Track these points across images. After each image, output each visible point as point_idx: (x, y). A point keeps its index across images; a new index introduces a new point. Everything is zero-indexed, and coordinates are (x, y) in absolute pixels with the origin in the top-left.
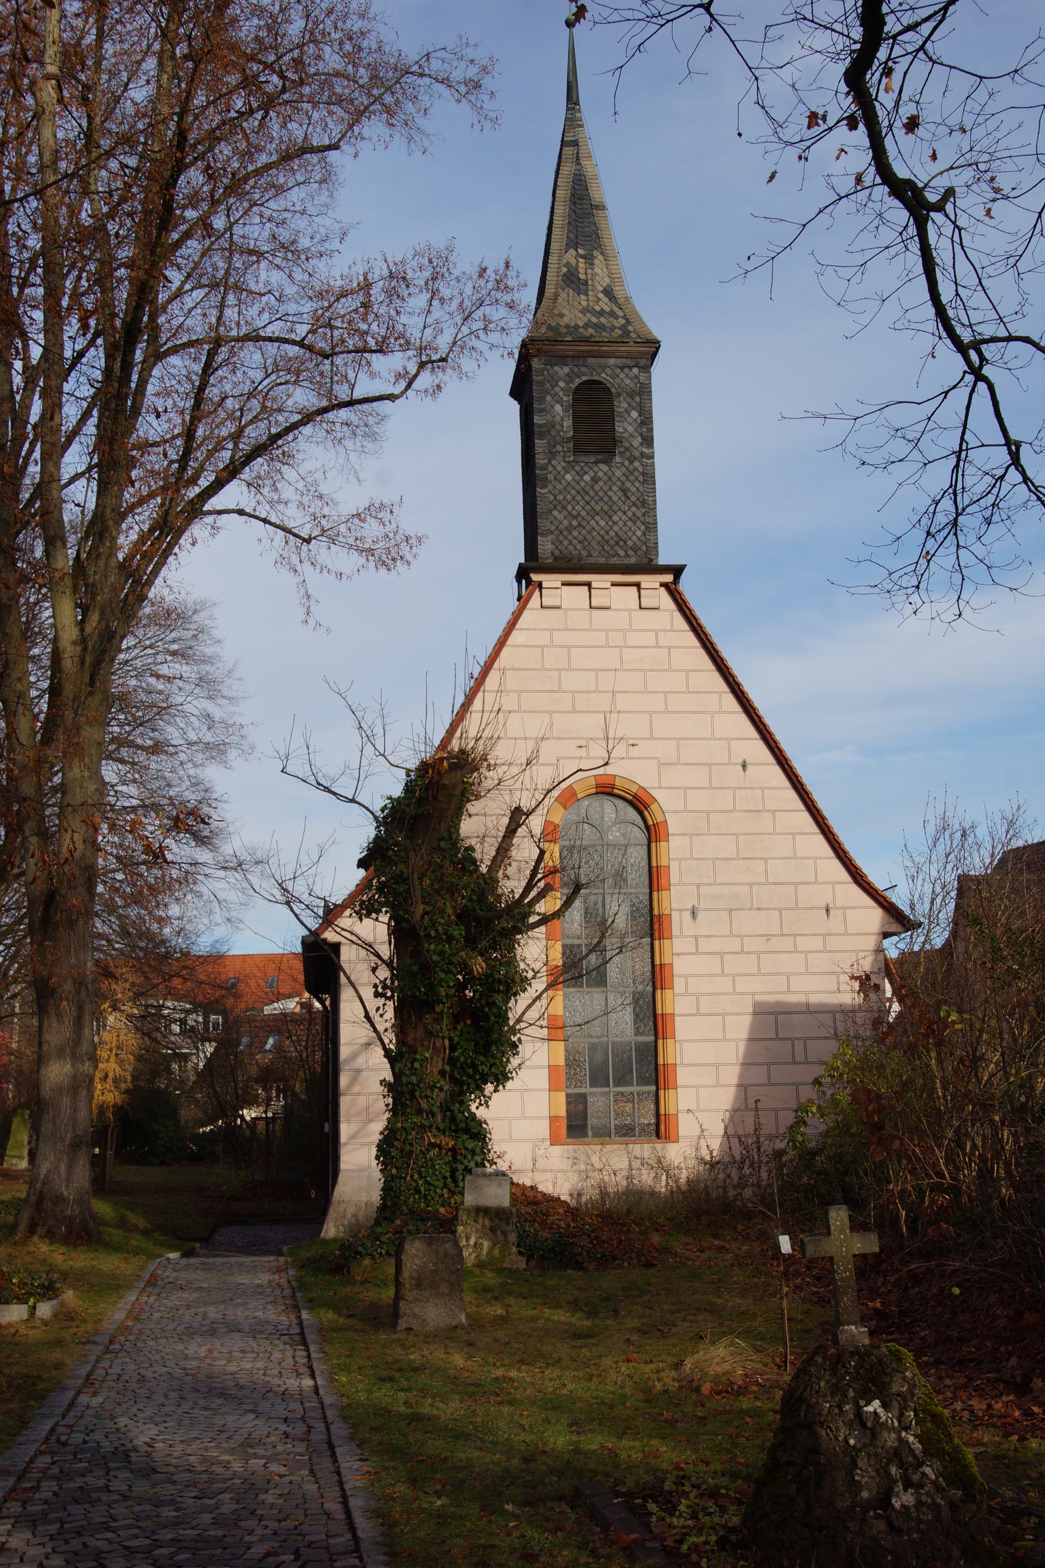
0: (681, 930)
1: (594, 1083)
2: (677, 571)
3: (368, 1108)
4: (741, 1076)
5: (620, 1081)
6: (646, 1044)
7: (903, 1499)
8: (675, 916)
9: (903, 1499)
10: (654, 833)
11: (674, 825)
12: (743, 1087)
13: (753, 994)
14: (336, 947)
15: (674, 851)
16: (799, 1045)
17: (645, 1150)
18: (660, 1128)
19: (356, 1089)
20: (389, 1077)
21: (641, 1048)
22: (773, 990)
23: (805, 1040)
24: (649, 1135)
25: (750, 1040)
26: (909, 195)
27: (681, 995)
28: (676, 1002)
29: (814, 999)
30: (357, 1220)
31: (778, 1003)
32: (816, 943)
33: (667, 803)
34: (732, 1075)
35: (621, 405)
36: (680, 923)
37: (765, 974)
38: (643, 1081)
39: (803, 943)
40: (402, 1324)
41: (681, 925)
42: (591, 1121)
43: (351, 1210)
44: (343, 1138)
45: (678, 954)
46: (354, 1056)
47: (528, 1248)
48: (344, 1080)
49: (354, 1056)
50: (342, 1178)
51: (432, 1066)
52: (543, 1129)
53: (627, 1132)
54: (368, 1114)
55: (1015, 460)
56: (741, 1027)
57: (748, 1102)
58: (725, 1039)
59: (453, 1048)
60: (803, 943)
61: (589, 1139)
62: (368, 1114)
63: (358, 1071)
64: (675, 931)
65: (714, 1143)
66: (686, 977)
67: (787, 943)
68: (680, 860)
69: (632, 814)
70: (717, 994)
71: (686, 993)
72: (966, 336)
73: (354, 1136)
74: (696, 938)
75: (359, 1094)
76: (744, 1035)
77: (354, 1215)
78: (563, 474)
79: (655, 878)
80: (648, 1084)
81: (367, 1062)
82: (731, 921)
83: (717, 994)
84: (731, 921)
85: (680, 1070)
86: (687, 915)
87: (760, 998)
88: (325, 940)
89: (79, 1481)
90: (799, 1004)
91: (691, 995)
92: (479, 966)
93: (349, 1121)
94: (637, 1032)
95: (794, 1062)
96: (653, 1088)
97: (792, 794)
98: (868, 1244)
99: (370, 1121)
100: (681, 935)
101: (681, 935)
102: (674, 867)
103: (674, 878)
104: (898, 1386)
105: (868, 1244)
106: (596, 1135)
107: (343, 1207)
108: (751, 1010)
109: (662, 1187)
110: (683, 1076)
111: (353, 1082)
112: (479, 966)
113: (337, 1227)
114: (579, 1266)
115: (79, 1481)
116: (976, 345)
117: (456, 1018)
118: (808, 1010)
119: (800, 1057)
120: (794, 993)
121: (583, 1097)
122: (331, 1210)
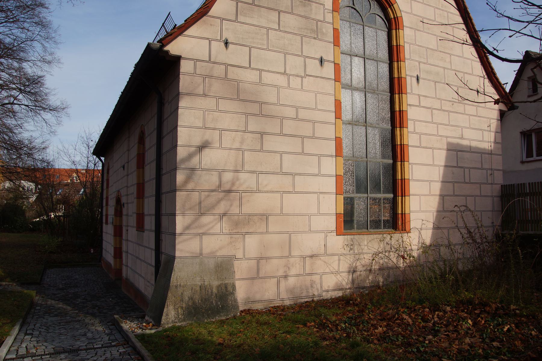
0: (412, 90)
3: (200, 203)
4: (441, 190)
6: (389, 164)
8: (408, 79)
11: (406, 20)
12: (442, 197)
13: (447, 137)
14: (177, 59)
19: (190, 186)
22: (453, 136)
23: (470, 168)
24: (363, 228)
25: (446, 166)
27: (412, 133)
28: (411, 137)
29: (474, 144)
30: (194, 303)
31: (458, 145)
34: (437, 188)
36: (410, 83)
37: (452, 126)
41: (411, 86)
42: (355, 218)
43: (187, 294)
45: (410, 105)
46: (190, 156)
48: (180, 177)
49: (190, 156)
50: (177, 264)
52: (331, 223)
54: (200, 208)
56: (441, 157)
58: (433, 165)
61: (355, 231)
62: (200, 208)
63: (193, 170)
64: (409, 91)
66: (414, 121)
68: (410, 44)
70: (430, 135)
71: (414, 132)
73: (188, 227)
74: (419, 96)
75: (193, 190)
76: (443, 163)
77: (191, 298)
80: (389, 193)
81: (200, 163)
82: (436, 88)
83: (430, 135)
84: (436, 88)
85: (412, 183)
86: (414, 80)
87: (450, 140)
88: (167, 52)
89: (31, 134)
90: (466, 146)
91: (417, 133)
93: (183, 214)
94: (384, 157)
95: (465, 183)
96: (391, 196)
99: (202, 214)
100: (411, 93)
101: (411, 93)
102: (407, 47)
106: (358, 228)
107: (180, 290)
108: (445, 147)
109: (401, 264)
111: (188, 179)
113: (176, 309)
115: (31, 134)
120: (464, 139)
121: (352, 199)
122: (170, 295)
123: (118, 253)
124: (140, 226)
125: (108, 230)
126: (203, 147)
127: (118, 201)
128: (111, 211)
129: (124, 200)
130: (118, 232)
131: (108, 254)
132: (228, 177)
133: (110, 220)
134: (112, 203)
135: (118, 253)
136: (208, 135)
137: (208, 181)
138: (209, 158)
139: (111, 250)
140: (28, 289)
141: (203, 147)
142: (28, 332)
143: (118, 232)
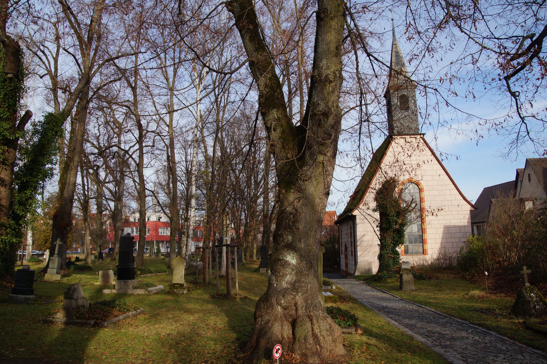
1: (410, 243)
2: (424, 134)
5: (415, 242)
7: (537, 307)
9: (537, 307)
10: (421, 190)
12: (442, 243)
15: (425, 194)
16: (453, 234)
17: (422, 257)
18: (424, 252)
20: (379, 243)
21: (419, 236)
26: (513, 94)
29: (456, 224)
32: (456, 213)
33: (423, 184)
34: (439, 241)
35: (410, 99)
38: (420, 242)
39: (453, 213)
40: (403, 289)
42: (409, 251)
44: (358, 255)
46: (360, 239)
47: (415, 276)
48: (358, 243)
51: (389, 241)
53: (417, 253)
55: (528, 133)
56: (441, 231)
57: (443, 247)
59: (394, 238)
60: (453, 213)
65: (435, 257)
67: (450, 213)
69: (416, 186)
72: (522, 116)
78: (398, 115)
79: (421, 200)
92: (400, 221)
97: (450, 181)
98: (529, 271)
103: (425, 199)
104: (535, 292)
105: (529, 271)
110: (428, 241)
112: (400, 221)
114: (425, 279)
116: (524, 118)
117: (393, 232)
118: (455, 227)
119: (453, 237)
123: (347, 265)
124: (352, 255)
125: (342, 256)
126: (364, 236)
127: (346, 246)
128: (343, 249)
129: (347, 246)
130: (346, 257)
131: (343, 267)
132: (370, 242)
133: (343, 253)
134: (344, 246)
135: (347, 265)
136: (365, 233)
137: (365, 244)
138: (365, 238)
139: (344, 265)
140: (403, 334)
141: (364, 236)
142: (156, 210)
143: (346, 257)
